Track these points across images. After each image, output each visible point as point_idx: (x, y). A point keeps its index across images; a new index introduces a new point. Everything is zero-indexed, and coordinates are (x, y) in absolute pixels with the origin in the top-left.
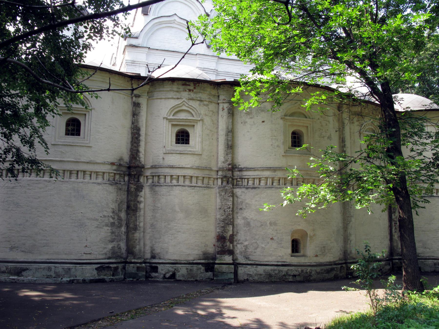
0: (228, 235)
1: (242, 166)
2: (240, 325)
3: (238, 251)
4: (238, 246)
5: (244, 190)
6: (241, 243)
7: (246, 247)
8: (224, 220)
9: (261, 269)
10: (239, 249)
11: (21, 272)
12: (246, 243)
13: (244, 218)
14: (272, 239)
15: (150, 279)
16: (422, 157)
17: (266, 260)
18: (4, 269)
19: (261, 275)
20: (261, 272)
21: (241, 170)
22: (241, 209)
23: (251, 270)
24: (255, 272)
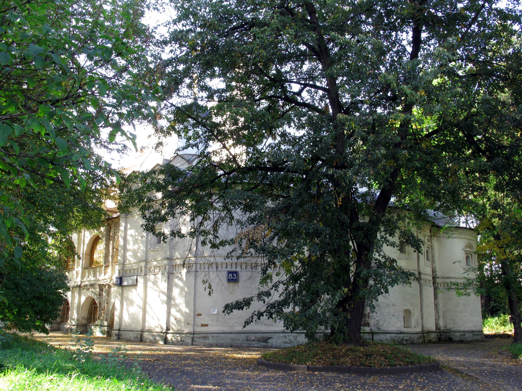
4: (372, 320)
7: (378, 321)
9: (388, 336)
11: (267, 340)
12: (377, 318)
14: (393, 315)
16: (286, 231)
17: (390, 329)
18: (254, 338)
20: (389, 338)
23: (382, 337)
24: (385, 338)
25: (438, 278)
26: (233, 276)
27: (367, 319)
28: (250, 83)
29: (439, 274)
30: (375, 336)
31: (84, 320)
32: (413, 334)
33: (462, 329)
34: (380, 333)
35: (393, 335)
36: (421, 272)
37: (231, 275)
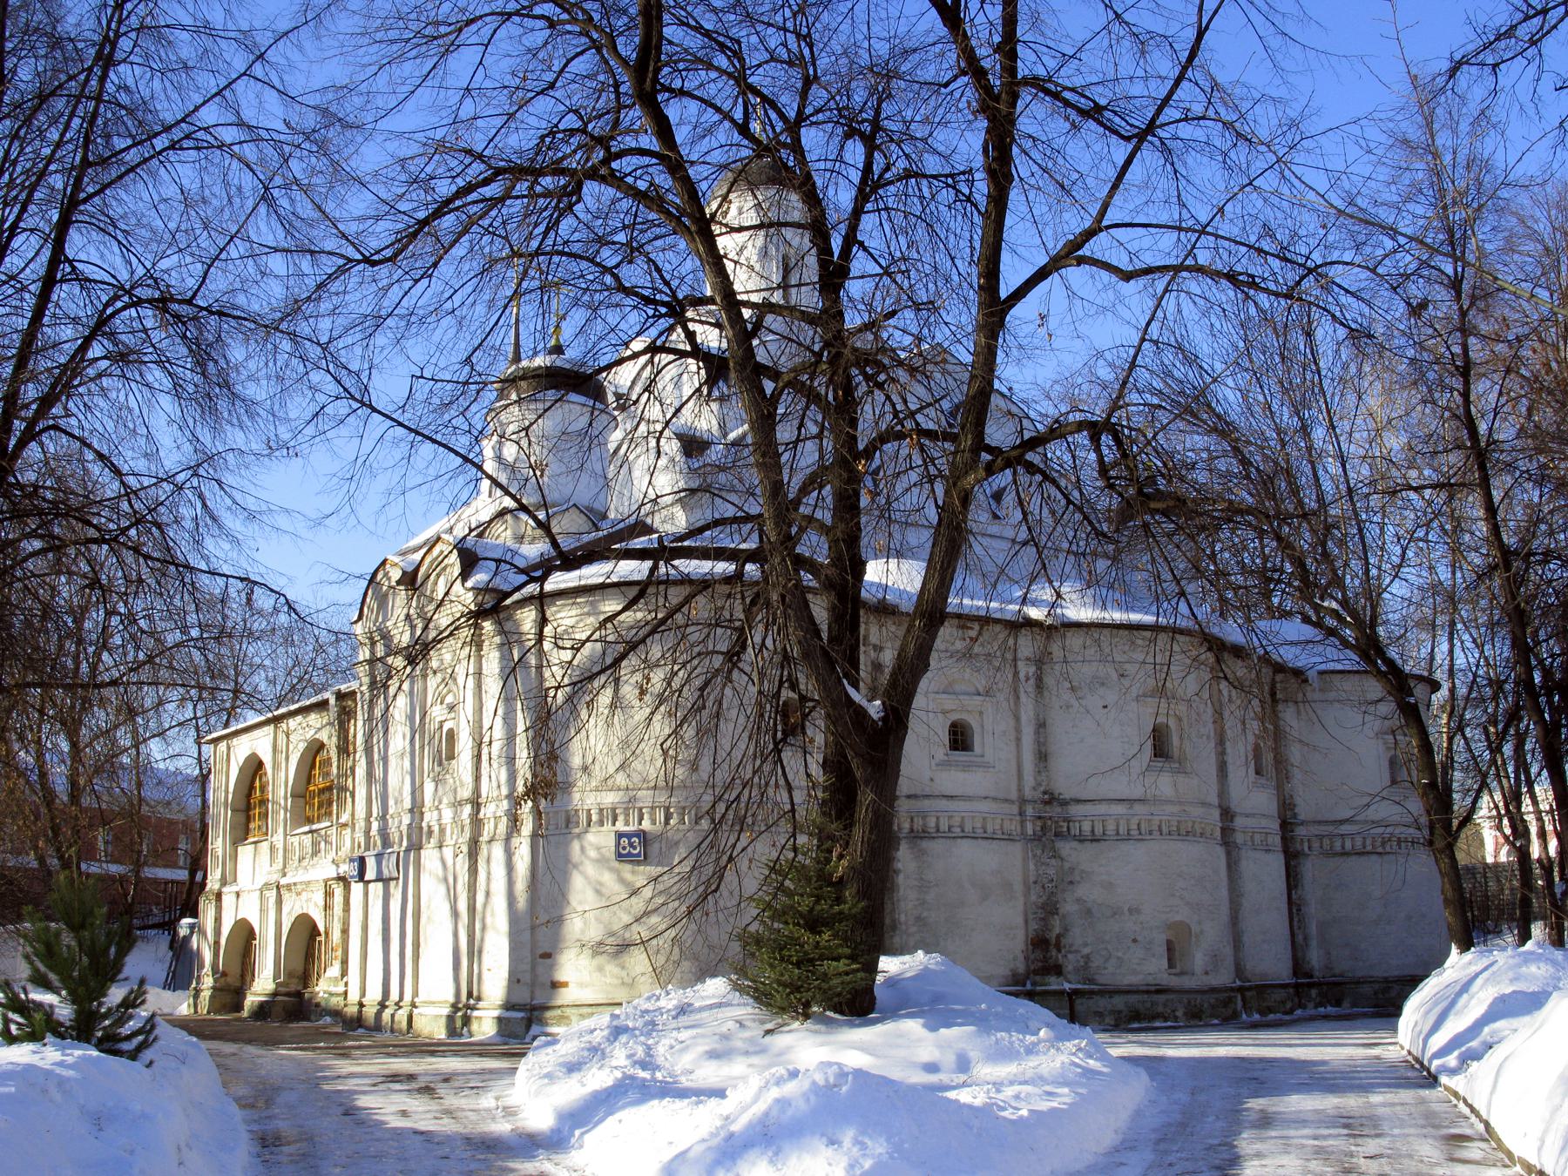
0: (1052, 936)
1: (1067, 796)
2: (1120, 1137)
3: (1070, 968)
4: (1070, 956)
5: (1075, 844)
6: (1077, 951)
7: (1087, 958)
8: (1043, 907)
10: (1070, 963)
12: (1086, 951)
13: (1078, 900)
14: (1135, 941)
15: (508, 602)
19: (1120, 1012)
20: (1121, 1006)
21: (1064, 803)
22: (1071, 882)
24: (1109, 1007)
25: (1302, 824)
26: (631, 845)
27: (1054, 952)
28: (19, 580)
29: (1304, 811)
30: (1078, 1001)
31: (295, 981)
32: (1148, 992)
33: (1378, 973)
34: (1092, 993)
35: (1133, 999)
36: (1234, 806)
37: (625, 841)
